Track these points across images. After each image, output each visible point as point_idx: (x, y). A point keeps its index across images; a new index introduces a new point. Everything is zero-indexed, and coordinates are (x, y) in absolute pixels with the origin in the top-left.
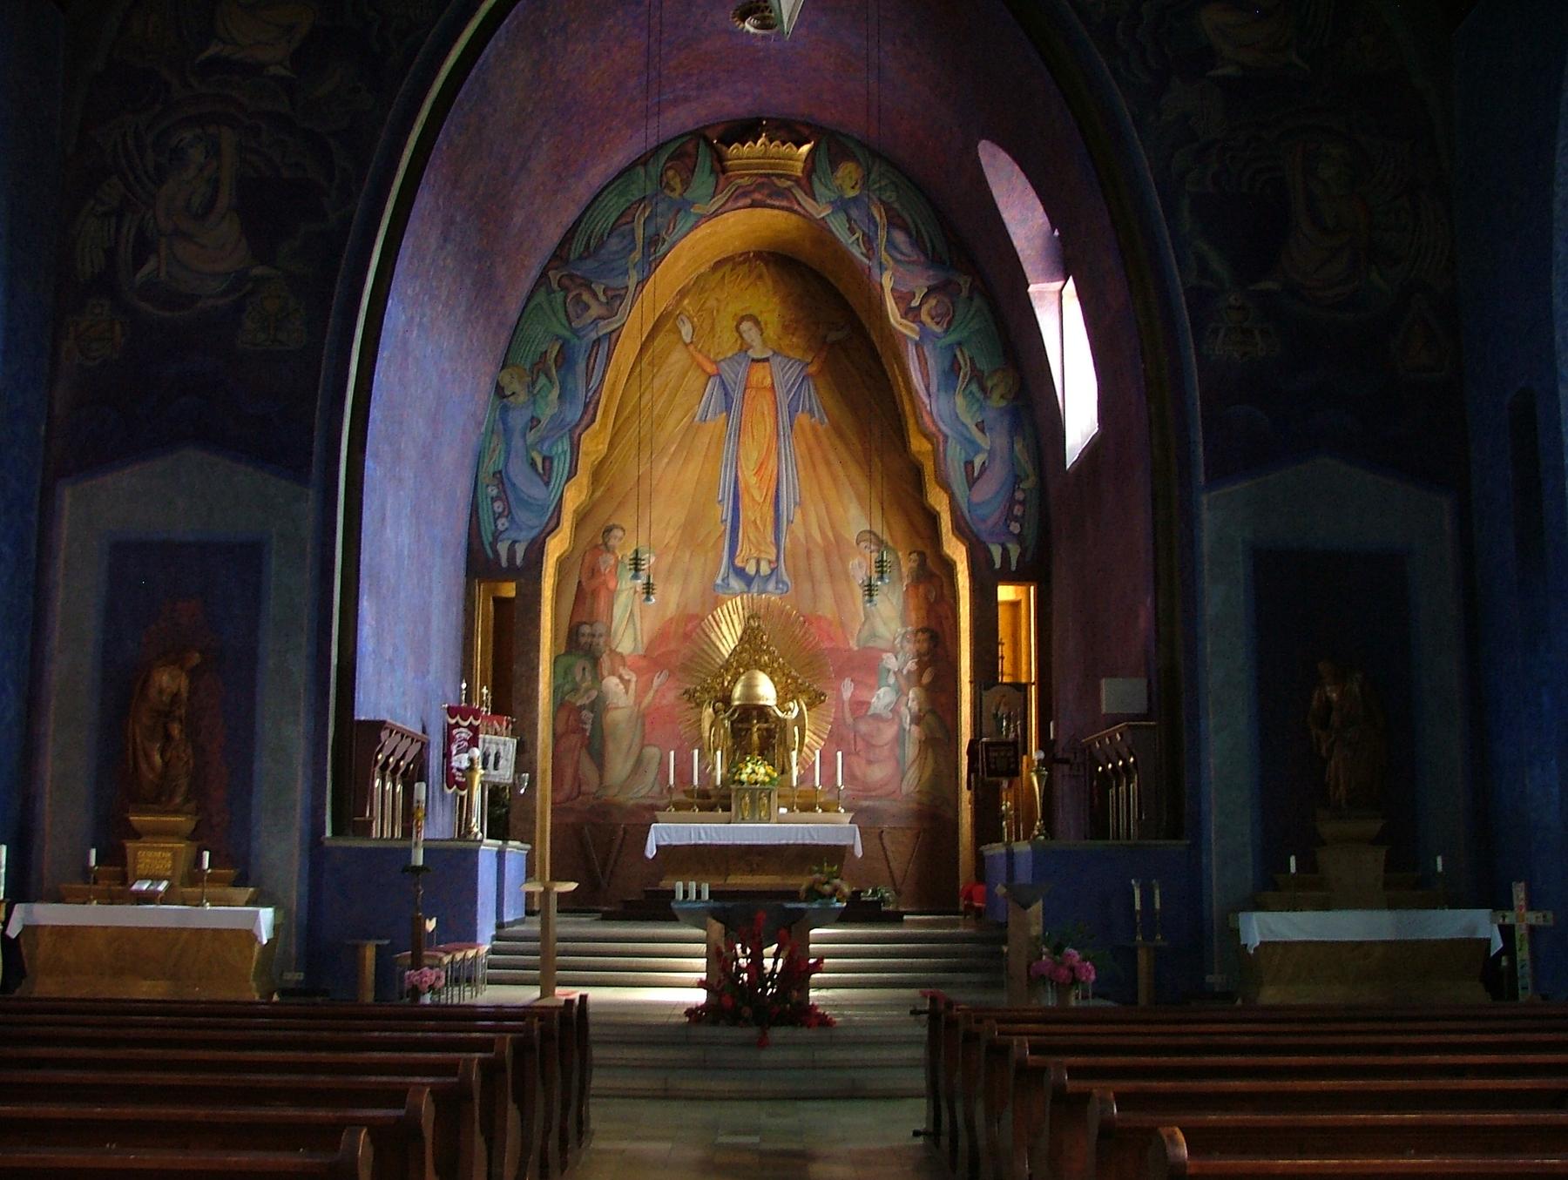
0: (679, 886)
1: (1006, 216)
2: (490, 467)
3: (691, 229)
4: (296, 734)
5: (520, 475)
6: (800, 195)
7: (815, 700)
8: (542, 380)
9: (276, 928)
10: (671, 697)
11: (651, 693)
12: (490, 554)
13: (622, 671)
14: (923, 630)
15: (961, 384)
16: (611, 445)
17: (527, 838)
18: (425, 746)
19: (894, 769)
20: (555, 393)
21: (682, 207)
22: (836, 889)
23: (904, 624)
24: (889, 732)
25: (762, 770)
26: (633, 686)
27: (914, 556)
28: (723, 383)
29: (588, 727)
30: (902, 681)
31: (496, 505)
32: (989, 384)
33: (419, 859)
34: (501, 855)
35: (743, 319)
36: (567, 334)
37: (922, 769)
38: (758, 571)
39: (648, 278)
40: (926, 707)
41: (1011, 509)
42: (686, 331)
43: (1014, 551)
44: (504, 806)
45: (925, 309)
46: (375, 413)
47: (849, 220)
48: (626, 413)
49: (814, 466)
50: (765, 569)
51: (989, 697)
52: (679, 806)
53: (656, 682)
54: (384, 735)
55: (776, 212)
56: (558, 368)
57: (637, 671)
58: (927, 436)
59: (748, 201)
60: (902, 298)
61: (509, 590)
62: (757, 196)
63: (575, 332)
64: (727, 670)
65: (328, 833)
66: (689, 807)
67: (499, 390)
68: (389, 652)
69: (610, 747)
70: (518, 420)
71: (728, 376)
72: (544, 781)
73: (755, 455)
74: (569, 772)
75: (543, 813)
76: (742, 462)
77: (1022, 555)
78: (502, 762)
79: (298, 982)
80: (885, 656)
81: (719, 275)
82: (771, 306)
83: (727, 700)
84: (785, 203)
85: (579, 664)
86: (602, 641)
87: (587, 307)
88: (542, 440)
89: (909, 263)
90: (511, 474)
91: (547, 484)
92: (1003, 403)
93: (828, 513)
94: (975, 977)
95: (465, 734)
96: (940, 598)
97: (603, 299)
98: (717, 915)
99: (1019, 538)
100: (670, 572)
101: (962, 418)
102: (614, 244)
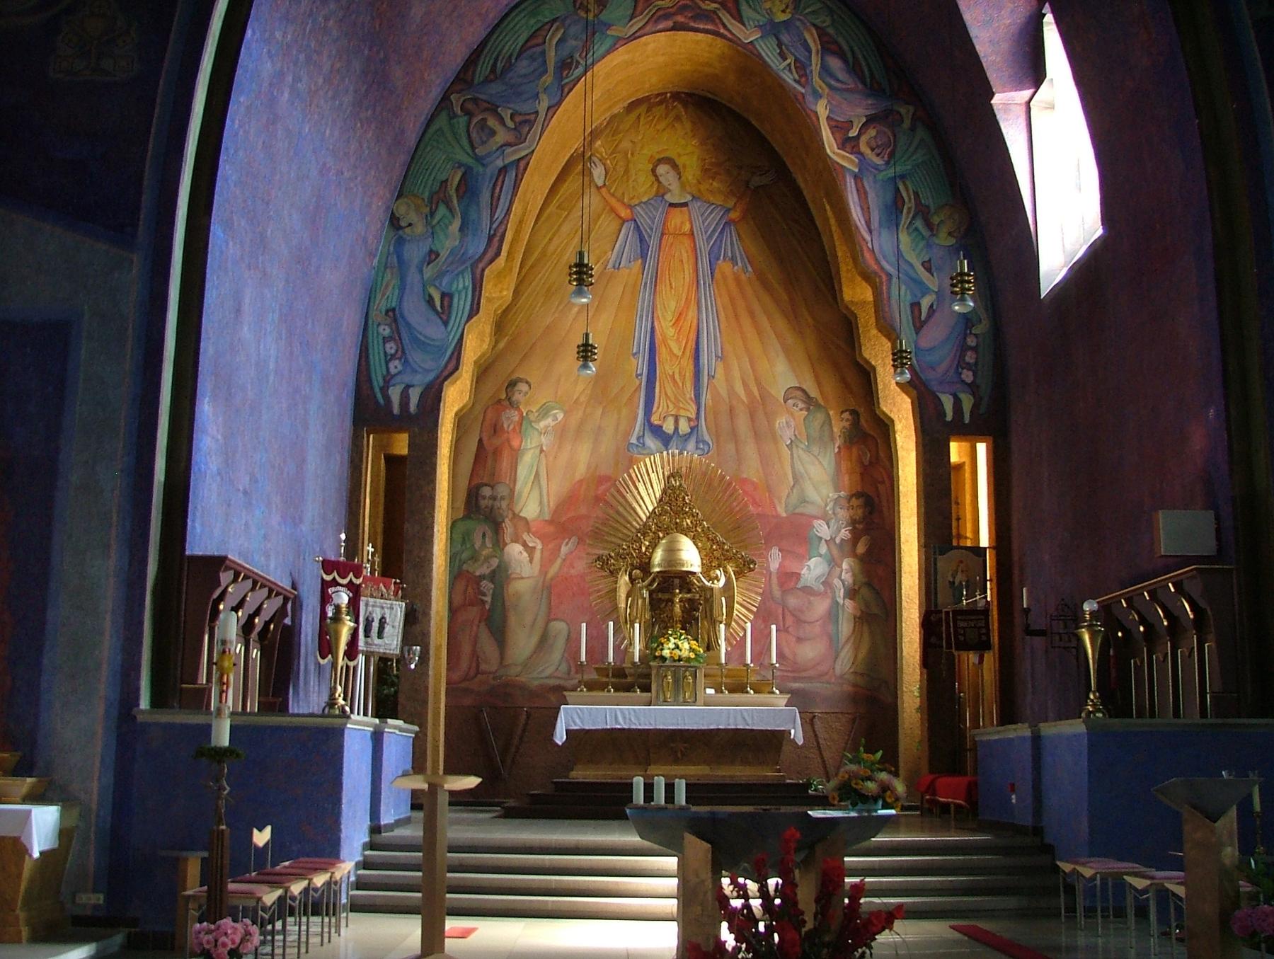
0: (639, 782)
1: (967, 17)
2: (381, 304)
3: (608, 52)
4: (105, 571)
5: (415, 312)
6: (726, 18)
7: (745, 568)
8: (442, 210)
9: (64, 834)
10: (581, 566)
11: (559, 561)
12: (381, 401)
13: (525, 537)
14: (858, 495)
15: (905, 219)
16: (517, 293)
17: (416, 716)
18: (297, 603)
19: (825, 646)
20: (456, 224)
21: (593, 30)
22: (885, 788)
23: (837, 489)
24: (821, 607)
25: (686, 646)
26: (537, 555)
27: (846, 415)
28: (637, 228)
29: (488, 599)
30: (835, 552)
31: (388, 346)
32: (936, 220)
33: (223, 737)
34: (377, 737)
35: (660, 161)
36: (470, 161)
37: (857, 649)
38: (676, 429)
39: (559, 104)
40: (861, 579)
41: (962, 356)
42: (598, 173)
43: (967, 402)
44: (393, 684)
45: (863, 139)
46: (227, 170)
47: (780, 45)
48: (530, 263)
49: (736, 316)
50: (684, 427)
51: (942, 562)
52: (591, 686)
53: (564, 550)
54: (226, 577)
55: (700, 36)
56: (460, 198)
57: (542, 537)
58: (867, 277)
59: (670, 23)
60: (839, 128)
61: (401, 444)
62: (680, 19)
63: (478, 159)
64: (644, 534)
65: (144, 703)
66: (602, 687)
67: (394, 222)
68: (244, 481)
69: (513, 620)
70: (415, 253)
71: (644, 221)
72: (438, 658)
73: (673, 305)
74: (466, 649)
75: (437, 694)
76: (659, 312)
77: (975, 407)
78: (388, 629)
79: (96, 907)
80: (816, 523)
81: (634, 115)
82: (689, 149)
83: (645, 567)
84: (709, 27)
85: (479, 530)
86: (504, 504)
87: (493, 133)
88: (441, 274)
89: (847, 90)
90: (406, 313)
91: (446, 323)
92: (952, 241)
93: (752, 367)
94: (1011, 902)
95: (344, 598)
96: (875, 461)
97: (511, 124)
98: (703, 828)
99: (973, 388)
100: (579, 431)
101: (908, 257)
102: (523, 66)
